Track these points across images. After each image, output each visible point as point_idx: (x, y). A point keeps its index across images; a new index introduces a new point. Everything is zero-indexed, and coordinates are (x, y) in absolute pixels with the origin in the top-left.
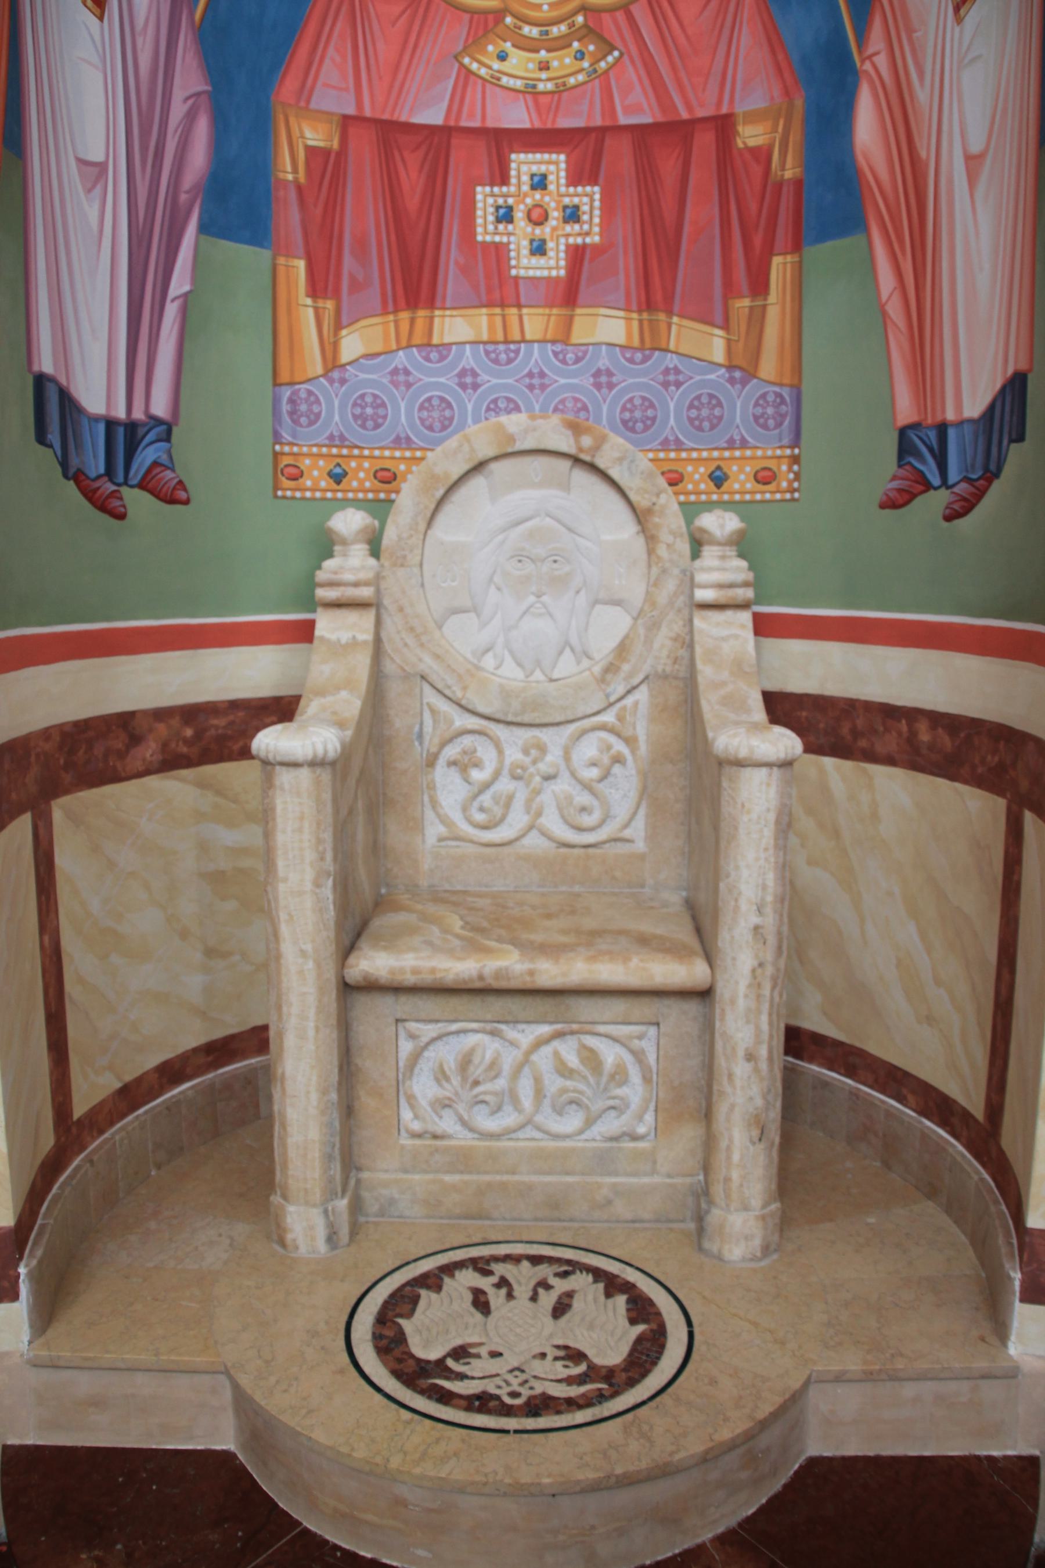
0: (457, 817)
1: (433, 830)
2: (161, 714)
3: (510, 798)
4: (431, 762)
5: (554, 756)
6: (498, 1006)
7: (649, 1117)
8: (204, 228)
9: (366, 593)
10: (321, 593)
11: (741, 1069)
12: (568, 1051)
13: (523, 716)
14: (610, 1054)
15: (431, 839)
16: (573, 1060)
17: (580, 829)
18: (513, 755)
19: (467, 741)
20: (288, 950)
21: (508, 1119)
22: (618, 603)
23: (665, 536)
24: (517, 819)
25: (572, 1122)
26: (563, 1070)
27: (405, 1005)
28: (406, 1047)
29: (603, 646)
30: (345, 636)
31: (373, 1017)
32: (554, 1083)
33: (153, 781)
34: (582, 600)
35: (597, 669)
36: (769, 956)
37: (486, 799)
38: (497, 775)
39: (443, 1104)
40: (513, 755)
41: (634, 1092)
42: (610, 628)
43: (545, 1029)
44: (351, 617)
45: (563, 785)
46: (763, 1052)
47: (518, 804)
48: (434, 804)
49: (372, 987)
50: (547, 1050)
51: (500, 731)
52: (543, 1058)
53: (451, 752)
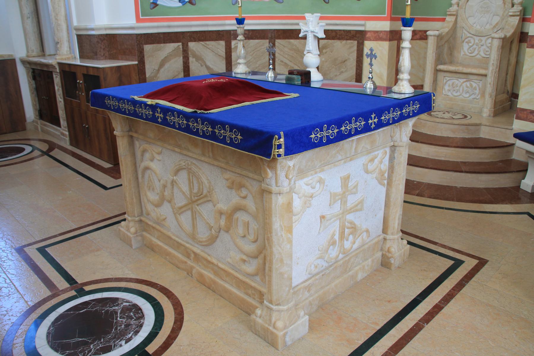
0: (466, 51)
1: (462, 53)
2: (420, 31)
3: (475, 49)
4: (463, 42)
5: (483, 42)
6: (458, 75)
7: (479, 96)
8: (99, 87)
9: (454, 13)
10: (448, 13)
11: (489, 86)
12: (468, 84)
13: (479, 35)
14: (474, 85)
15: (462, 55)
16: (469, 85)
17: (486, 55)
18: (477, 41)
19: (469, 38)
20: (428, 62)
21: (458, 94)
22: (498, 15)
23: (507, 3)
24: (476, 52)
25: (467, 95)
26: (467, 87)
27: (446, 74)
28: (445, 81)
29: (494, 22)
30: (450, 20)
31: (440, 75)
32: (465, 89)
33: (418, 41)
34: (492, 15)
35: (492, 27)
36: (494, 68)
37: (471, 49)
38: (473, 45)
39: (449, 90)
40: (477, 41)
41: (477, 92)
42: (496, 19)
43: (465, 80)
44: (452, 17)
45: (484, 47)
46: (492, 83)
47: (476, 50)
48: (463, 49)
49: (441, 71)
50: (465, 83)
51: (475, 37)
52: (464, 84)
53: (466, 40)
